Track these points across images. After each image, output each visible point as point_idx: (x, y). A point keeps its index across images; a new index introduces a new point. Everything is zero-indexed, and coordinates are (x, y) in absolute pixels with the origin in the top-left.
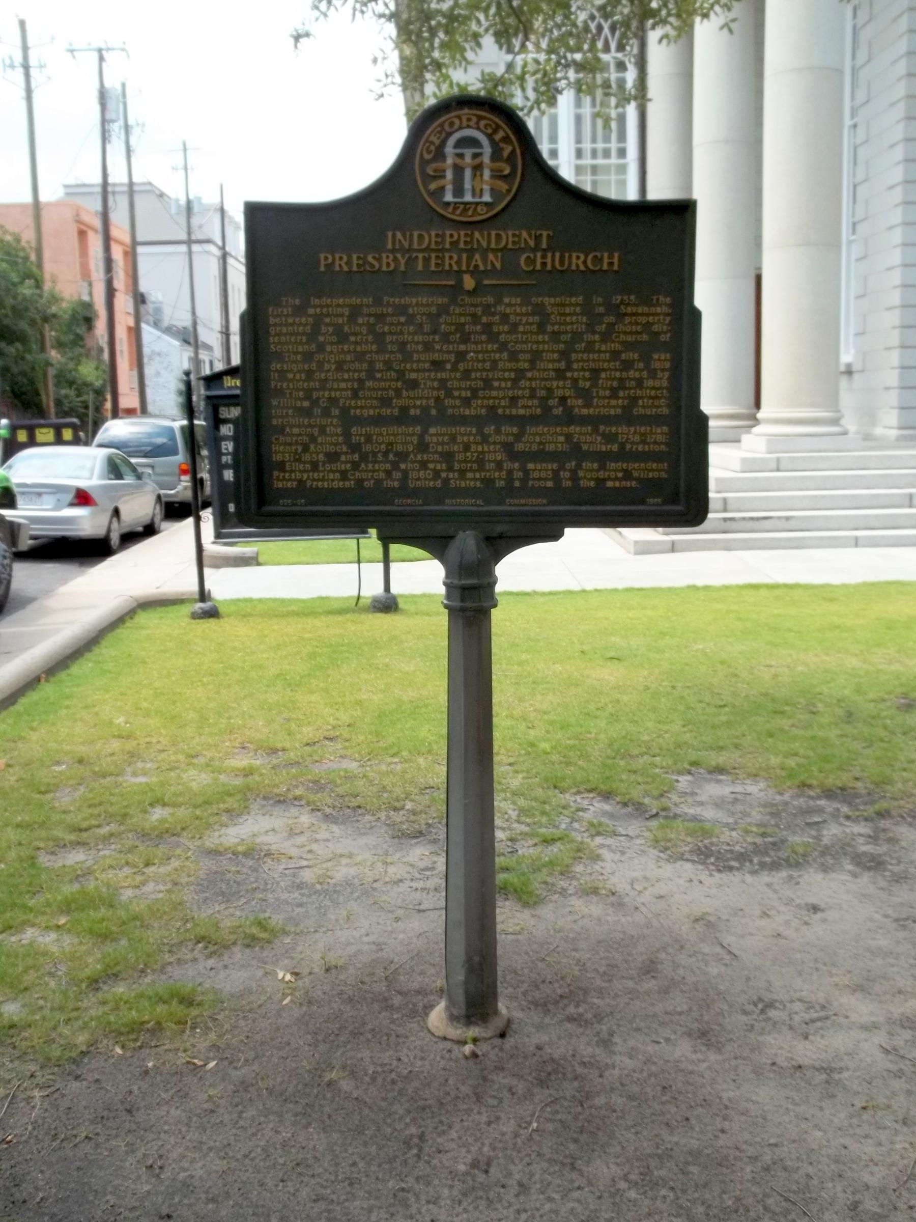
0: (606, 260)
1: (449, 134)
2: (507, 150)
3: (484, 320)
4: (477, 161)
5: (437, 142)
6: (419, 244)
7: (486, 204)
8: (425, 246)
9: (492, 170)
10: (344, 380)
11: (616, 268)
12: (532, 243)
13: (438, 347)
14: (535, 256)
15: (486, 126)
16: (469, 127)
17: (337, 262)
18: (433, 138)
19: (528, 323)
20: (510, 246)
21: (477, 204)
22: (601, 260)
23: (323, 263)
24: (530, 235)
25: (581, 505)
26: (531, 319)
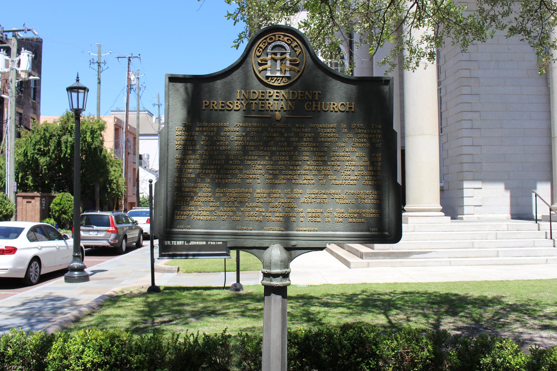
0: (314, 105)
1: (269, 44)
2: (298, 50)
3: (286, 135)
4: (283, 56)
5: (263, 47)
6: (292, 97)
7: (288, 77)
8: (296, 97)
9: (290, 61)
10: (212, 164)
11: (353, 110)
12: (311, 98)
13: (262, 148)
14: (312, 104)
15: (288, 40)
16: (279, 40)
17: (212, 105)
18: (261, 45)
19: (308, 137)
20: (299, 98)
21: (283, 77)
22: (312, 106)
23: (204, 105)
24: (310, 93)
25: (336, 231)
26: (310, 135)
